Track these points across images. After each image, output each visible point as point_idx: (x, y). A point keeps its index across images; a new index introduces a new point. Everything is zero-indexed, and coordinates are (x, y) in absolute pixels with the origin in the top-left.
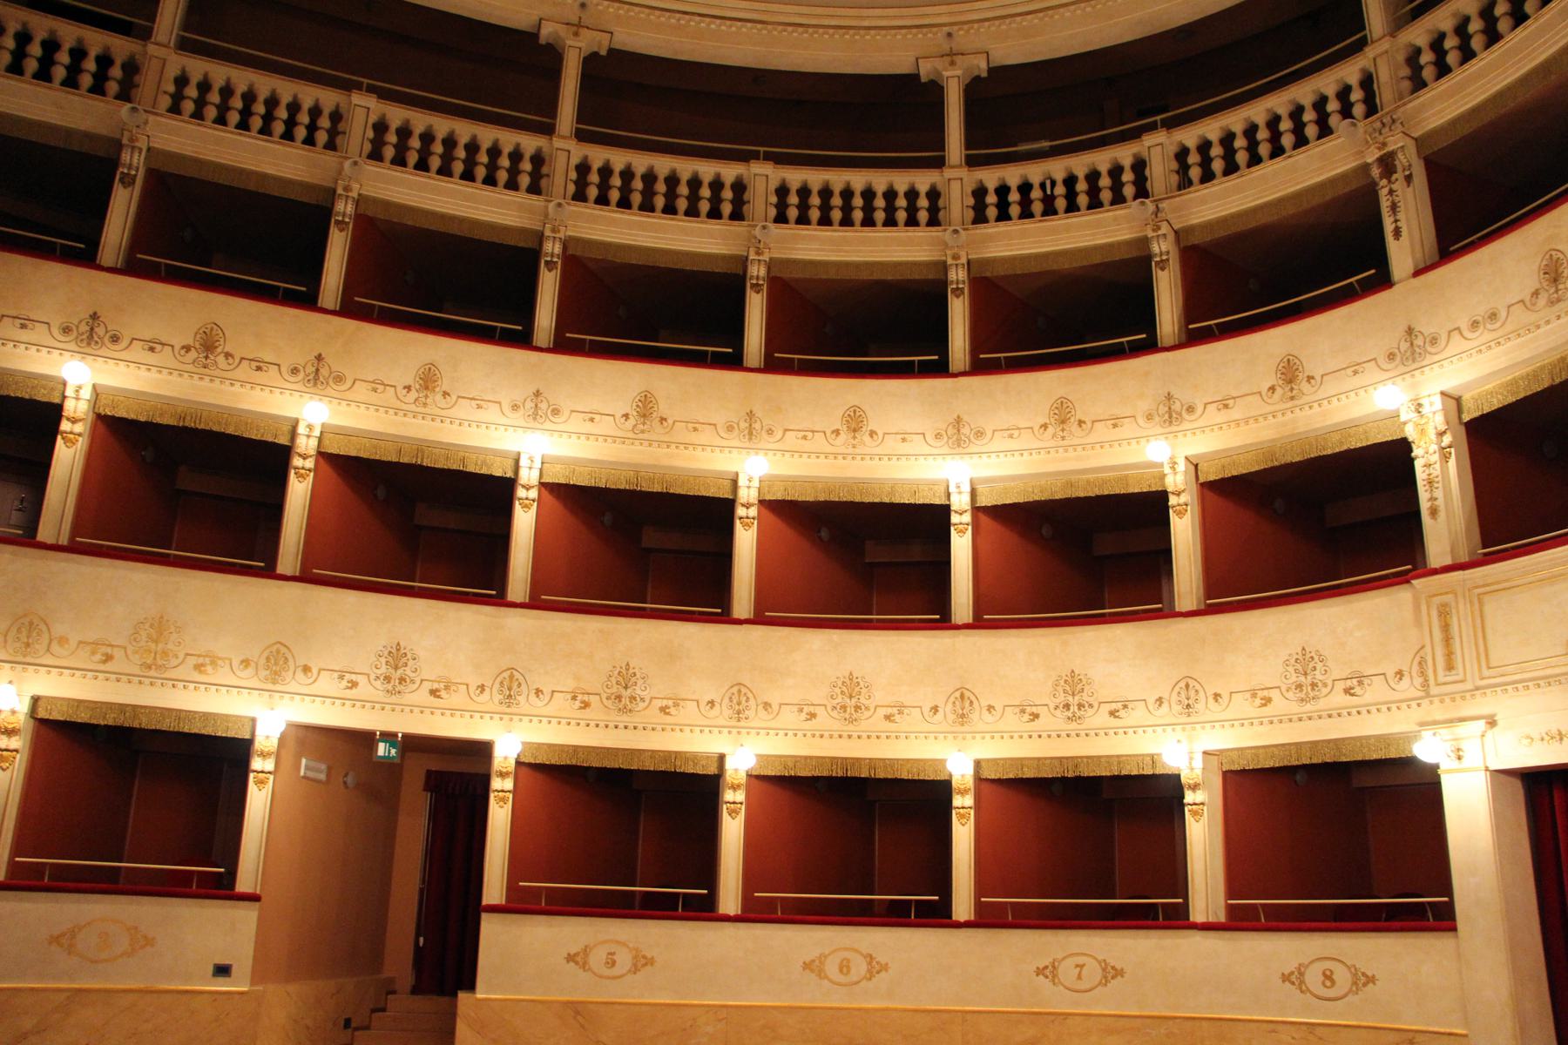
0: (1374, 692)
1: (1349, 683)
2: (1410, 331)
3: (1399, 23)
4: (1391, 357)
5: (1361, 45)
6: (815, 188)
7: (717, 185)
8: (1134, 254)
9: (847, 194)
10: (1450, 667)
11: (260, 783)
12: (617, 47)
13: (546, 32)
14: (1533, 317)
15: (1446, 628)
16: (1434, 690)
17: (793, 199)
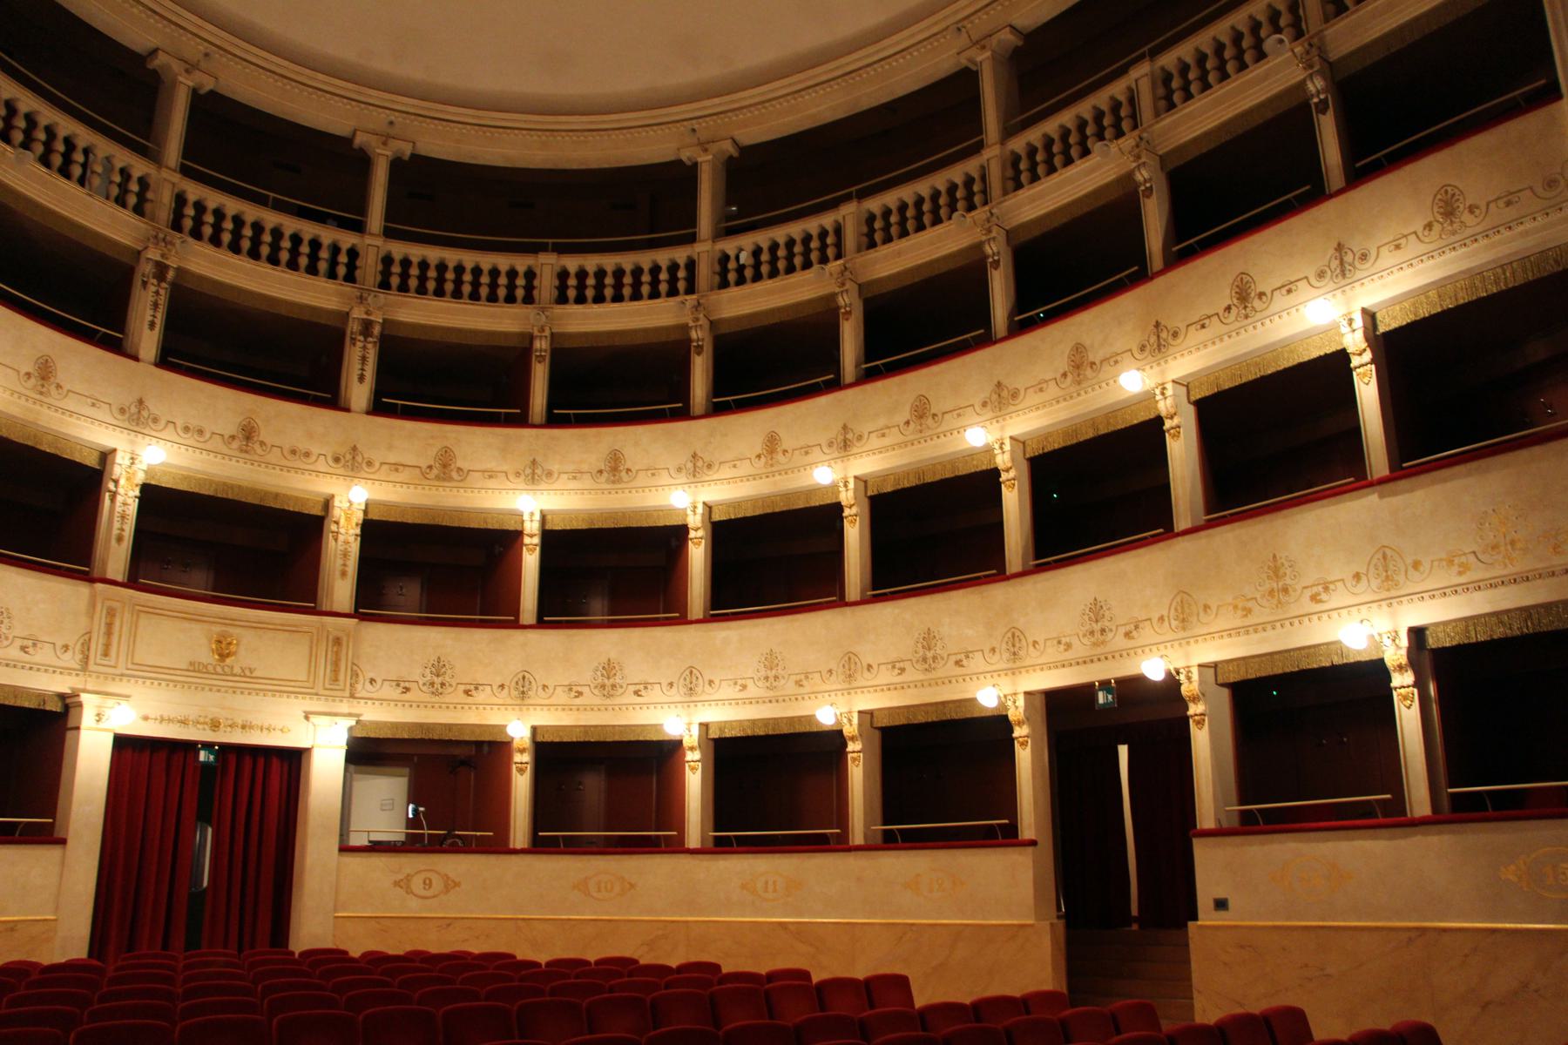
0: (43, 655)
1: (26, 642)
2: (141, 402)
3: (1008, 132)
4: (122, 411)
5: (978, 148)
6: (415, 260)
7: (512, 274)
8: (125, 259)
9: (459, 269)
10: (106, 654)
11: (1200, 723)
12: (423, 153)
13: (360, 140)
14: (225, 450)
15: (109, 626)
16: (92, 667)
17: (396, 269)
